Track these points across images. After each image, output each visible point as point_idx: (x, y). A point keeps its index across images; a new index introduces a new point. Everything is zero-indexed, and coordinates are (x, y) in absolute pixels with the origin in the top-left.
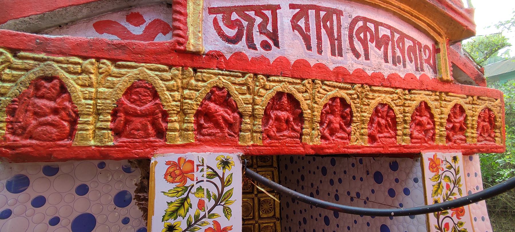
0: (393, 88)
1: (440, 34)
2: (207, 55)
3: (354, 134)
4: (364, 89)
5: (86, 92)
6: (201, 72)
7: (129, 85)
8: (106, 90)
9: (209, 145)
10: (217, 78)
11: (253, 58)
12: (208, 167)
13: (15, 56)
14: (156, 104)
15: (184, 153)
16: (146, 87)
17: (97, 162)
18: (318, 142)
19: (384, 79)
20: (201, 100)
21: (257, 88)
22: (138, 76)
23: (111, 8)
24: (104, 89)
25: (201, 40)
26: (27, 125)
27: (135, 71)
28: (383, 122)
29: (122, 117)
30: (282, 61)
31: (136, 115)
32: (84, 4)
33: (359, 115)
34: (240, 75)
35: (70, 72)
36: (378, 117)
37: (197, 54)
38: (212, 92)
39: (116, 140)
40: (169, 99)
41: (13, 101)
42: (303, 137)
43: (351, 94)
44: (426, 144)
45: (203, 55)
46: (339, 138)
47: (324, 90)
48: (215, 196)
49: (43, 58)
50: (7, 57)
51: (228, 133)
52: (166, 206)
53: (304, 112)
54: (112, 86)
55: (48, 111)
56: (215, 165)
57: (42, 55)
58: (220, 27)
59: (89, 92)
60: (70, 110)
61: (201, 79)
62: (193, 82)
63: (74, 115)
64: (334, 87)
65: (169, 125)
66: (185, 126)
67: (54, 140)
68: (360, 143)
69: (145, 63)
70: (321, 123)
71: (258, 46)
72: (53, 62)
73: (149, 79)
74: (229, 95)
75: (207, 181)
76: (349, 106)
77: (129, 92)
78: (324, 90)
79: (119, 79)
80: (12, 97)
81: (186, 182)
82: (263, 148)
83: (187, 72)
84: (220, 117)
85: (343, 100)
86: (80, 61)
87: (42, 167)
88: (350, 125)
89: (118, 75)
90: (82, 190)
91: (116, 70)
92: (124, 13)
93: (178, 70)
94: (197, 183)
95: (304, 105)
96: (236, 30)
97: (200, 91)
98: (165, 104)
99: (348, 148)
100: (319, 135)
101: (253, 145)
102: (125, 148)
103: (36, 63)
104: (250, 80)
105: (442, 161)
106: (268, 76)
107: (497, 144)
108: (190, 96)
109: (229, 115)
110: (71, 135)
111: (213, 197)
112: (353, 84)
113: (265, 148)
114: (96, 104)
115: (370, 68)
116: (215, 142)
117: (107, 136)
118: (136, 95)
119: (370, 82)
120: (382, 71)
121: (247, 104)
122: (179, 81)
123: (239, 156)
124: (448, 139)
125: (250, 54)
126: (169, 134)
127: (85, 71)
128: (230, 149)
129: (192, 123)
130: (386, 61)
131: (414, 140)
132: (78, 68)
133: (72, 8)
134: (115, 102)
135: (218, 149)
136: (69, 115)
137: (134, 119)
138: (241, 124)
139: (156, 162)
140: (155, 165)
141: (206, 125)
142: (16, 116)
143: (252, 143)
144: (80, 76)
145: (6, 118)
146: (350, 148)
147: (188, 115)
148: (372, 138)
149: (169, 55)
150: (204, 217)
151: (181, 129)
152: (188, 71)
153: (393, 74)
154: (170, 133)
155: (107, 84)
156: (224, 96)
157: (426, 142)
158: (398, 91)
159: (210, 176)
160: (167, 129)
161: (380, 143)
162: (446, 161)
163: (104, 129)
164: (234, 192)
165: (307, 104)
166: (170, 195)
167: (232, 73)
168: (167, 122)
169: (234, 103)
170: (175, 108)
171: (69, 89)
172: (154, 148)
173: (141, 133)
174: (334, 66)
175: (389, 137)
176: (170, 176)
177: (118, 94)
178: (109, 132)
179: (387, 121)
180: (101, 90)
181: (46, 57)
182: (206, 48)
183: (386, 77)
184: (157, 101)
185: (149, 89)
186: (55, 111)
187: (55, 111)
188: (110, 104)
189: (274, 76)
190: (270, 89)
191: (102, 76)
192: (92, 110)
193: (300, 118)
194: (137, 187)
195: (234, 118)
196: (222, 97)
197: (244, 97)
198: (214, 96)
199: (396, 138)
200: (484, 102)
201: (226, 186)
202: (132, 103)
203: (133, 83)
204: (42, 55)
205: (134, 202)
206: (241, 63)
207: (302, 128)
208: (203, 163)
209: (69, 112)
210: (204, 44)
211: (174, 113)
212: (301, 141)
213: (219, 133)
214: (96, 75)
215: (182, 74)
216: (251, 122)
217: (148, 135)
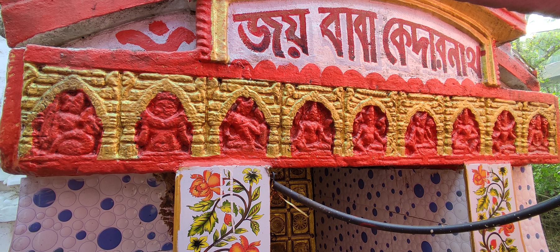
0: (432, 94)
1: (485, 35)
2: (232, 64)
3: (390, 144)
5: (110, 105)
6: (226, 82)
7: (153, 97)
8: (130, 102)
9: (236, 158)
10: (243, 88)
11: (280, 66)
12: (235, 181)
13: (40, 70)
14: (181, 116)
15: (209, 166)
16: (170, 99)
17: (121, 176)
18: (350, 153)
19: (422, 85)
20: (227, 111)
21: (285, 97)
23: (134, 18)
25: (225, 49)
26: (53, 139)
27: (159, 82)
28: (422, 131)
29: (146, 129)
30: (311, 69)
31: (160, 127)
32: (106, 14)
33: (395, 124)
34: (267, 84)
35: (94, 85)
36: (417, 126)
37: (221, 63)
38: (238, 102)
40: (193, 110)
42: (335, 148)
43: (386, 102)
44: (470, 155)
45: (228, 64)
46: (373, 149)
47: (357, 98)
48: (242, 210)
49: (67, 71)
50: (33, 72)
51: (255, 145)
52: (192, 221)
54: (136, 99)
57: (67, 69)
58: (245, 34)
59: (113, 105)
60: (95, 124)
61: (226, 89)
62: (218, 92)
63: (98, 129)
64: (368, 95)
65: (194, 137)
66: (210, 138)
67: (79, 154)
68: (396, 154)
69: (169, 74)
70: (354, 133)
71: (286, 53)
72: (77, 75)
73: (173, 91)
74: (256, 105)
75: (234, 195)
76: (384, 115)
77: (152, 104)
78: (357, 98)
79: (142, 91)
80: (38, 112)
81: (484, 185)
82: (292, 160)
83: (212, 83)
84: (247, 129)
85: (377, 108)
86: (104, 73)
87: (68, 181)
88: (386, 135)
89: (142, 87)
90: (108, 204)
91: (139, 82)
92: (147, 22)
93: (203, 81)
94: (223, 197)
95: (335, 114)
96: (263, 37)
97: (226, 102)
98: (189, 116)
99: (383, 159)
101: (281, 158)
103: (61, 76)
104: (277, 89)
105: (488, 173)
106: (296, 85)
108: (215, 107)
109: (256, 126)
110: (96, 149)
111: (240, 211)
112: (388, 91)
114: (120, 117)
115: (406, 74)
116: (241, 155)
117: (131, 149)
118: (160, 107)
119: (407, 89)
120: (420, 77)
122: (204, 92)
123: (266, 169)
124: (495, 148)
125: (277, 62)
126: (194, 147)
127: (108, 84)
129: (217, 135)
130: (425, 66)
131: (456, 151)
133: (95, 19)
134: (139, 114)
135: (244, 161)
136: (93, 128)
137: (158, 131)
138: (268, 135)
139: (181, 176)
143: (280, 155)
144: (104, 89)
146: (385, 160)
147: (213, 127)
148: (410, 149)
149: (193, 65)
150: (231, 231)
152: (213, 81)
153: (432, 80)
154: (195, 146)
156: (250, 107)
157: (470, 153)
158: (438, 97)
159: (236, 190)
160: (192, 142)
161: (419, 154)
163: (128, 142)
165: (339, 114)
166: (196, 209)
167: (258, 82)
168: (192, 135)
169: (261, 113)
171: (93, 102)
172: (179, 161)
173: (165, 146)
176: (196, 189)
177: (142, 106)
178: (134, 145)
179: (427, 130)
180: (124, 102)
181: (70, 70)
182: (230, 57)
183: (424, 83)
184: (182, 113)
185: (173, 100)
186: (80, 125)
187: (80, 125)
188: (134, 116)
189: (303, 84)
190: (298, 98)
191: (125, 88)
192: (116, 123)
193: (331, 128)
194: (162, 201)
195: (261, 129)
196: (248, 107)
197: (271, 107)
198: (240, 106)
199: (436, 149)
200: (535, 108)
202: (156, 115)
203: (157, 95)
204: (67, 69)
205: (159, 216)
206: (268, 71)
207: (333, 139)
208: (229, 176)
209: (93, 125)
211: (199, 125)
212: (332, 153)
213: (245, 145)
214: (120, 88)
215: (207, 85)
217: (173, 148)
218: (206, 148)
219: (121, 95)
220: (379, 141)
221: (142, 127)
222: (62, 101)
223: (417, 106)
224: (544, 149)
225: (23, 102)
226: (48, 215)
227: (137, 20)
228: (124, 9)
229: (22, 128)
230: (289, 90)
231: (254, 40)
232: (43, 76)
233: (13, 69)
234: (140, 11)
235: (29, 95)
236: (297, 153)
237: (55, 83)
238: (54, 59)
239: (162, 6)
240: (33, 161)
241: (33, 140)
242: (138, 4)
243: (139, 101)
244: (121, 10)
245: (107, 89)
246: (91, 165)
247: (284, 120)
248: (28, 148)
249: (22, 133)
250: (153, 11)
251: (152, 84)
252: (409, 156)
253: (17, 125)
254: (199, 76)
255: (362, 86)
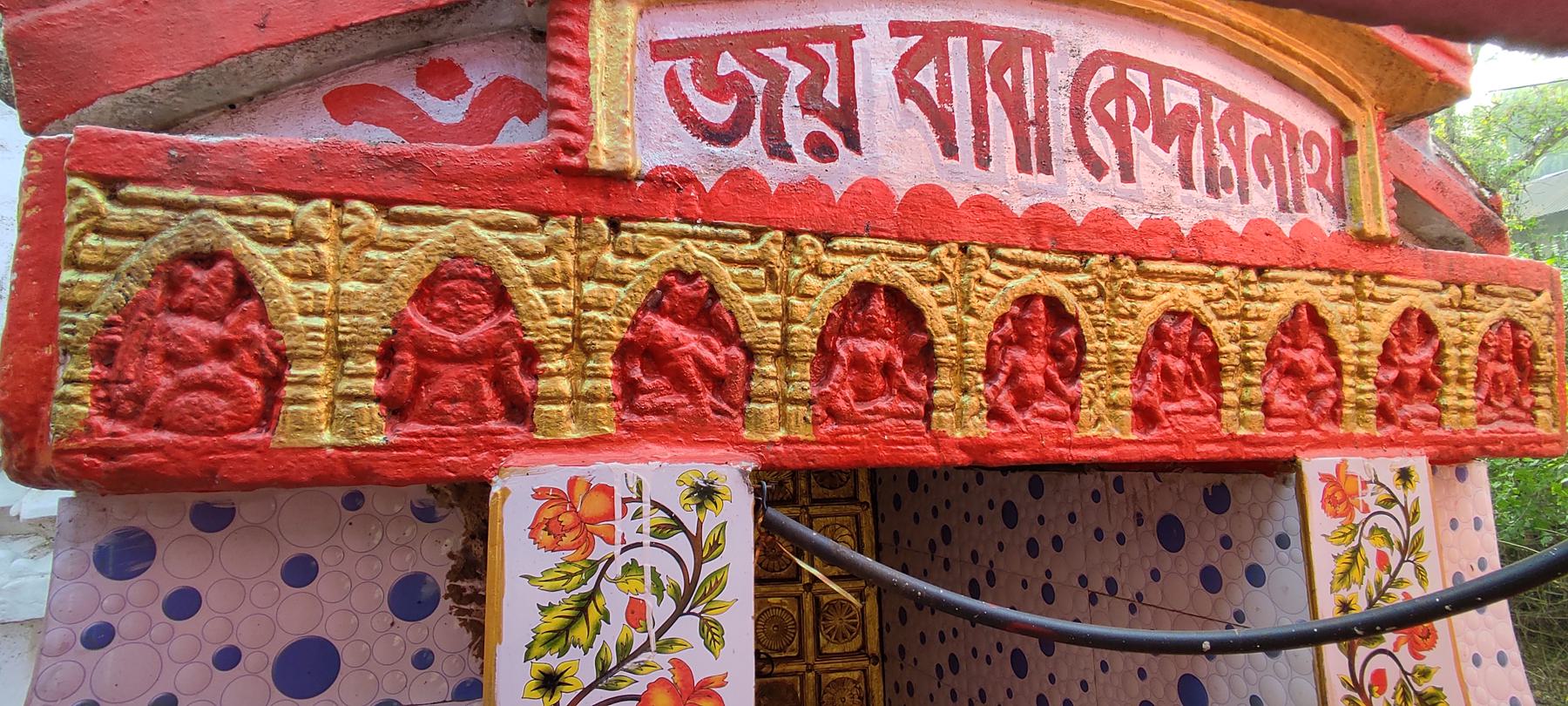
0: (1208, 263)
1: (1354, 98)
2: (648, 179)
3: (1090, 403)
4: (1119, 268)
5: (308, 294)
6: (632, 230)
7: (426, 273)
8: (363, 287)
10: (679, 247)
11: (781, 185)
12: (656, 505)
13: (112, 197)
14: (504, 324)
16: (475, 278)
17: (339, 493)
18: (978, 428)
19: (1180, 238)
20: (633, 311)
21: (797, 272)
22: (452, 245)
24: (356, 284)
25: (629, 137)
26: (147, 389)
27: (444, 231)
28: (1178, 365)
29: (408, 362)
30: (870, 193)
31: (448, 356)
33: (1103, 346)
34: (746, 235)
35: (262, 240)
36: (1165, 352)
37: (618, 178)
38: (664, 287)
39: (391, 428)
40: (540, 308)
41: (109, 324)
42: (934, 414)
43: (1078, 286)
44: (1312, 433)
45: (637, 179)
46: (1042, 415)
47: (998, 273)
48: (676, 588)
49: (186, 201)
50: (92, 202)
51: (711, 405)
52: (536, 618)
53: (937, 340)
54: (379, 276)
55: (203, 349)
56: (677, 500)
57: (186, 193)
58: (684, 96)
59: (316, 293)
60: (265, 347)
61: (631, 251)
62: (609, 258)
63: (274, 360)
64: (1028, 265)
65: (542, 384)
66: (588, 385)
67: (221, 431)
68: (1107, 430)
69: (470, 207)
70: (989, 373)
71: (798, 149)
72: (214, 212)
73: (482, 254)
74: (714, 295)
75: (652, 544)
76: (1073, 321)
77: (426, 292)
78: (998, 273)
79: (398, 255)
80: (105, 313)
81: (591, 546)
82: (815, 448)
83: (590, 232)
84: (689, 361)
86: (289, 206)
88: (1078, 377)
90: (301, 572)
91: (389, 230)
92: (412, 61)
93: (566, 226)
94: (623, 550)
95: (937, 319)
97: (630, 285)
98: (529, 324)
99: (1070, 445)
100: (982, 407)
101: (786, 441)
102: (419, 452)
103: (169, 214)
104: (775, 250)
105: (1364, 484)
106: (827, 237)
107: (1541, 431)
108: (600, 300)
109: (715, 352)
110: (267, 416)
111: (671, 590)
112: (1083, 255)
113: (823, 448)
115: (1135, 206)
117: (367, 418)
118: (448, 300)
119: (1138, 249)
120: (1173, 215)
121: (766, 319)
122: (569, 258)
123: (743, 472)
124: (1384, 414)
125: (775, 173)
126: (541, 411)
127: (303, 235)
128: (719, 452)
129: (606, 377)
130: (1188, 183)
131: (1274, 422)
132: (285, 227)
134: (389, 321)
135: (682, 451)
136: (261, 360)
137: (441, 368)
138: (749, 378)
140: (504, 500)
141: (648, 383)
142: (119, 366)
143: (782, 433)
144: (290, 250)
145: (90, 370)
148: (1145, 416)
149: (538, 183)
150: (645, 647)
151: (576, 396)
154: (546, 408)
155: (366, 270)
156: (699, 298)
157: (1314, 427)
158: (1225, 272)
159: (660, 531)
160: (535, 397)
161: (1170, 431)
162: (1377, 482)
163: (358, 398)
164: (731, 575)
165: (946, 317)
166: (547, 585)
167: (721, 231)
168: (536, 377)
169: (728, 318)
170: (557, 336)
171: (259, 287)
172: (500, 449)
173: (462, 408)
174: (1026, 202)
175: (1198, 413)
176: (546, 530)
177: (396, 298)
178: (373, 405)
179: (1192, 363)
180: (349, 286)
181: (195, 198)
182: (644, 160)
183: (1186, 233)
184: (507, 317)
185: (482, 281)
186: (223, 350)
187: (223, 350)
188: (373, 326)
189: (847, 235)
190: (833, 276)
191: (350, 247)
193: (925, 359)
194: (453, 562)
195: (729, 361)
196: (692, 300)
197: (757, 299)
198: (671, 298)
199: (1218, 415)
200: (1497, 300)
201: (709, 558)
202: (435, 322)
203: (439, 267)
204: (186, 193)
205: (445, 604)
206: (747, 199)
207: (931, 389)
208: (640, 492)
209: (260, 350)
210: (639, 149)
211: (556, 351)
212: (928, 428)
214: (334, 246)
215: (578, 238)
216: (779, 371)
217: (482, 415)
218: (574, 415)
219: (338, 268)
220: (1060, 394)
221: (398, 356)
222: (174, 284)
223: (1164, 297)
224: (1523, 415)
225: (65, 286)
226: (133, 602)
227: (382, 57)
228: (347, 28)
229: (61, 358)
230: (808, 251)
231: (708, 113)
232: (119, 214)
233: (35, 195)
234: (392, 30)
235: (82, 267)
236: (829, 429)
237: (153, 234)
238: (149, 166)
239: (453, 17)
240: (91, 452)
241: (93, 391)
242: (384, 13)
243: (389, 283)
244: (339, 28)
245: (300, 249)
246: (252, 461)
247: (794, 334)
248: (79, 413)
249: (61, 373)
250: (428, 33)
251: (424, 235)
252: (1144, 437)
253: (48, 351)
254: (556, 214)
255: (1011, 241)
